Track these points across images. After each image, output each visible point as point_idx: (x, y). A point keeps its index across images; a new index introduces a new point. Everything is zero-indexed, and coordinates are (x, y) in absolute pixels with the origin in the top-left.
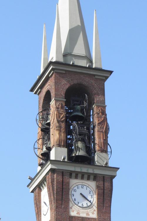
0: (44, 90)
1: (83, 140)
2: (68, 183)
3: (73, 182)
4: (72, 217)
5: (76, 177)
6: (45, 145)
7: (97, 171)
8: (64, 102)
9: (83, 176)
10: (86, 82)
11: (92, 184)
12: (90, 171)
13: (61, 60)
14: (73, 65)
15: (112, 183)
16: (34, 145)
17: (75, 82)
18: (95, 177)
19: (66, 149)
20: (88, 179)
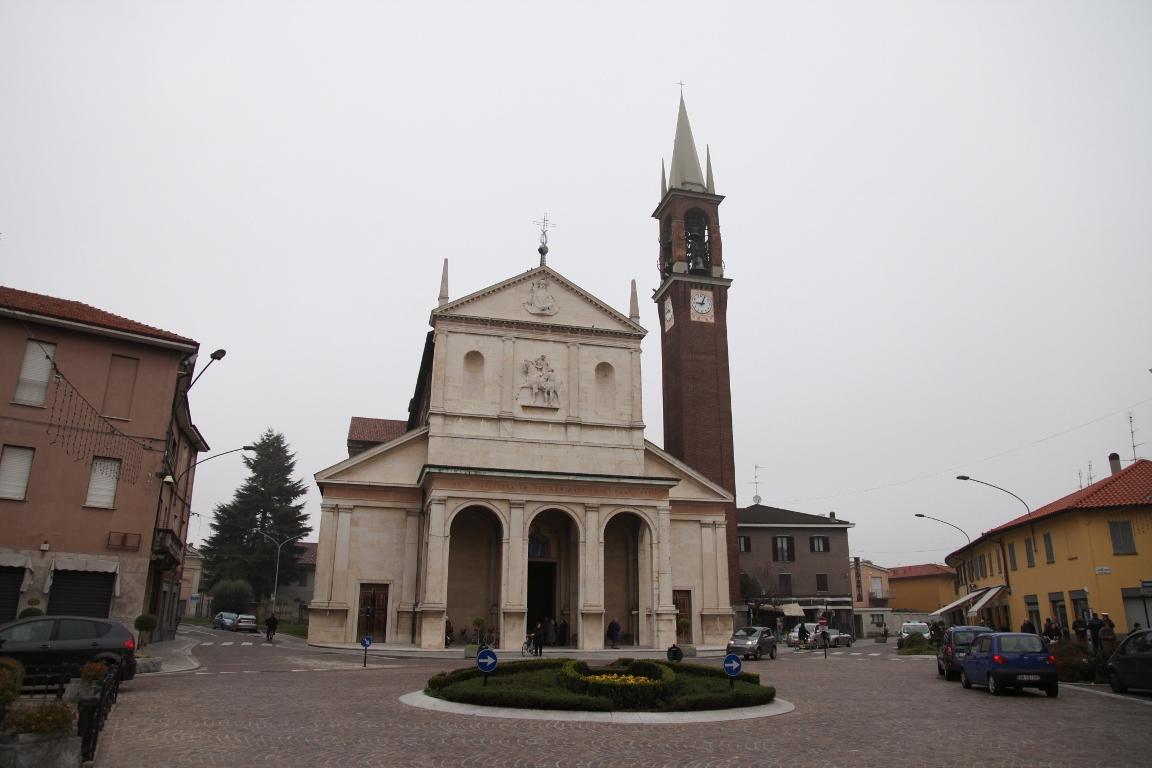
0: (666, 214)
1: (701, 256)
2: (690, 293)
3: (693, 292)
4: (694, 322)
5: (696, 288)
6: (186, 363)
7: (714, 283)
8: (684, 653)
9: (702, 287)
10: (702, 206)
11: (710, 294)
12: (708, 282)
13: (680, 187)
14: (690, 191)
15: (662, 241)
16: (15, 419)
17: (690, 207)
18: (712, 288)
19: (658, 221)
20: (706, 289)
